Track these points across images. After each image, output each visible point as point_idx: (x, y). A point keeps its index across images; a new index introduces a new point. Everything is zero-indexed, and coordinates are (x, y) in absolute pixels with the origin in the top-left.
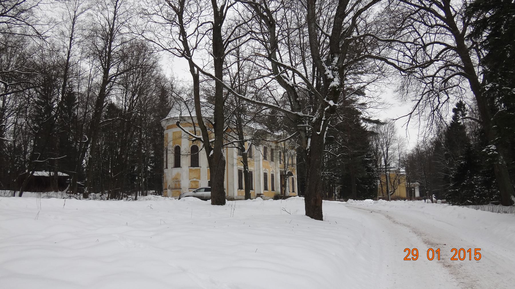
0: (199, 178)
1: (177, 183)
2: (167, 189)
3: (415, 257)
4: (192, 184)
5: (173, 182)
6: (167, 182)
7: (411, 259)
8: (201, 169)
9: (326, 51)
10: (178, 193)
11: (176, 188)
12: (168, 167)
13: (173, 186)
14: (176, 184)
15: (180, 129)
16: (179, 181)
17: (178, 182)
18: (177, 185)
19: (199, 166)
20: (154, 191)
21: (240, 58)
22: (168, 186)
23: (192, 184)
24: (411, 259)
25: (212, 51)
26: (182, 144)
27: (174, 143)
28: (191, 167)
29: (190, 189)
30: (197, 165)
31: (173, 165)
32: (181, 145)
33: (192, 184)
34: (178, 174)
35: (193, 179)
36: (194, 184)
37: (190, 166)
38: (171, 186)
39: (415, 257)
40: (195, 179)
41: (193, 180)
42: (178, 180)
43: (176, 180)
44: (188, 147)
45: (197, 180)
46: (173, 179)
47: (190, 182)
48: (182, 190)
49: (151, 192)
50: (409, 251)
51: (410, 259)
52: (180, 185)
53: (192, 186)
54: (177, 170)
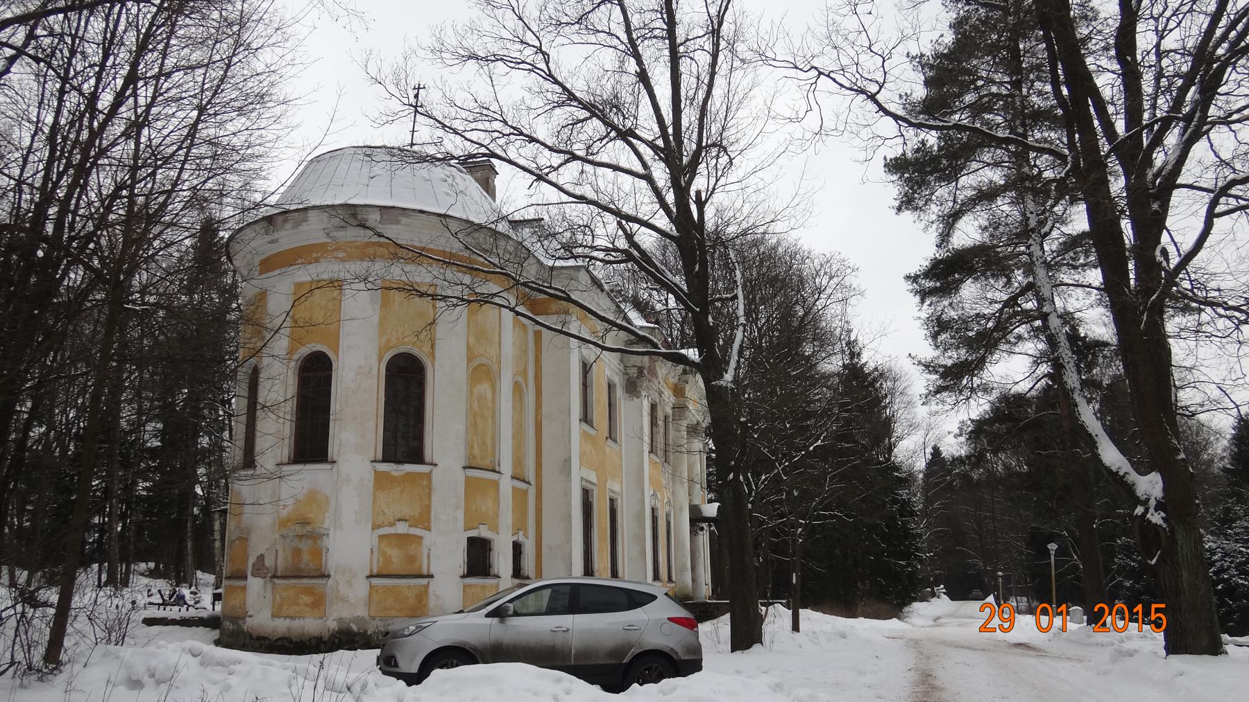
0: (424, 520)
1: (305, 546)
2: (245, 578)
3: (1006, 625)
4: (384, 554)
5: (282, 536)
6: (244, 540)
7: (998, 630)
8: (437, 474)
9: (1004, 249)
10: (306, 599)
11: (295, 574)
12: (259, 460)
13: (280, 559)
14: (297, 552)
15: (377, 366)
16: (316, 536)
17: (310, 542)
18: (306, 557)
19: (427, 458)
20: (152, 565)
21: (1047, 618)
22: (252, 560)
23: (389, 551)
24: (998, 630)
25: (674, 228)
26: (344, 342)
27: (296, 341)
28: (385, 460)
29: (375, 581)
30: (416, 455)
31: (285, 450)
32: (337, 352)
33: (384, 554)
34: (314, 498)
35: (391, 525)
36: (395, 554)
37: (380, 456)
38: (269, 562)
39: (1006, 625)
40: (402, 528)
41: (392, 530)
42: (309, 528)
43: (299, 530)
44: (375, 357)
45: (414, 531)
46: (284, 523)
47: (376, 542)
48: (331, 581)
49: (143, 566)
50: (991, 607)
51: (994, 630)
52: (318, 554)
53: (388, 560)
54: (311, 475)
